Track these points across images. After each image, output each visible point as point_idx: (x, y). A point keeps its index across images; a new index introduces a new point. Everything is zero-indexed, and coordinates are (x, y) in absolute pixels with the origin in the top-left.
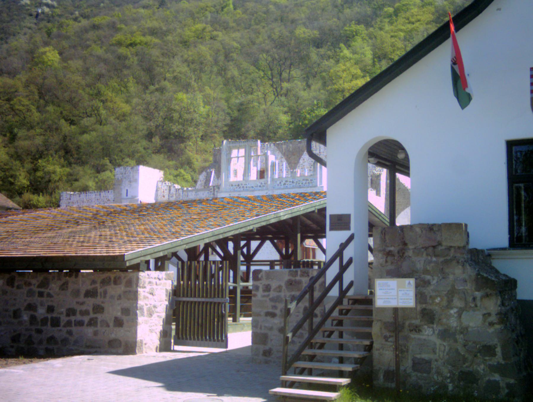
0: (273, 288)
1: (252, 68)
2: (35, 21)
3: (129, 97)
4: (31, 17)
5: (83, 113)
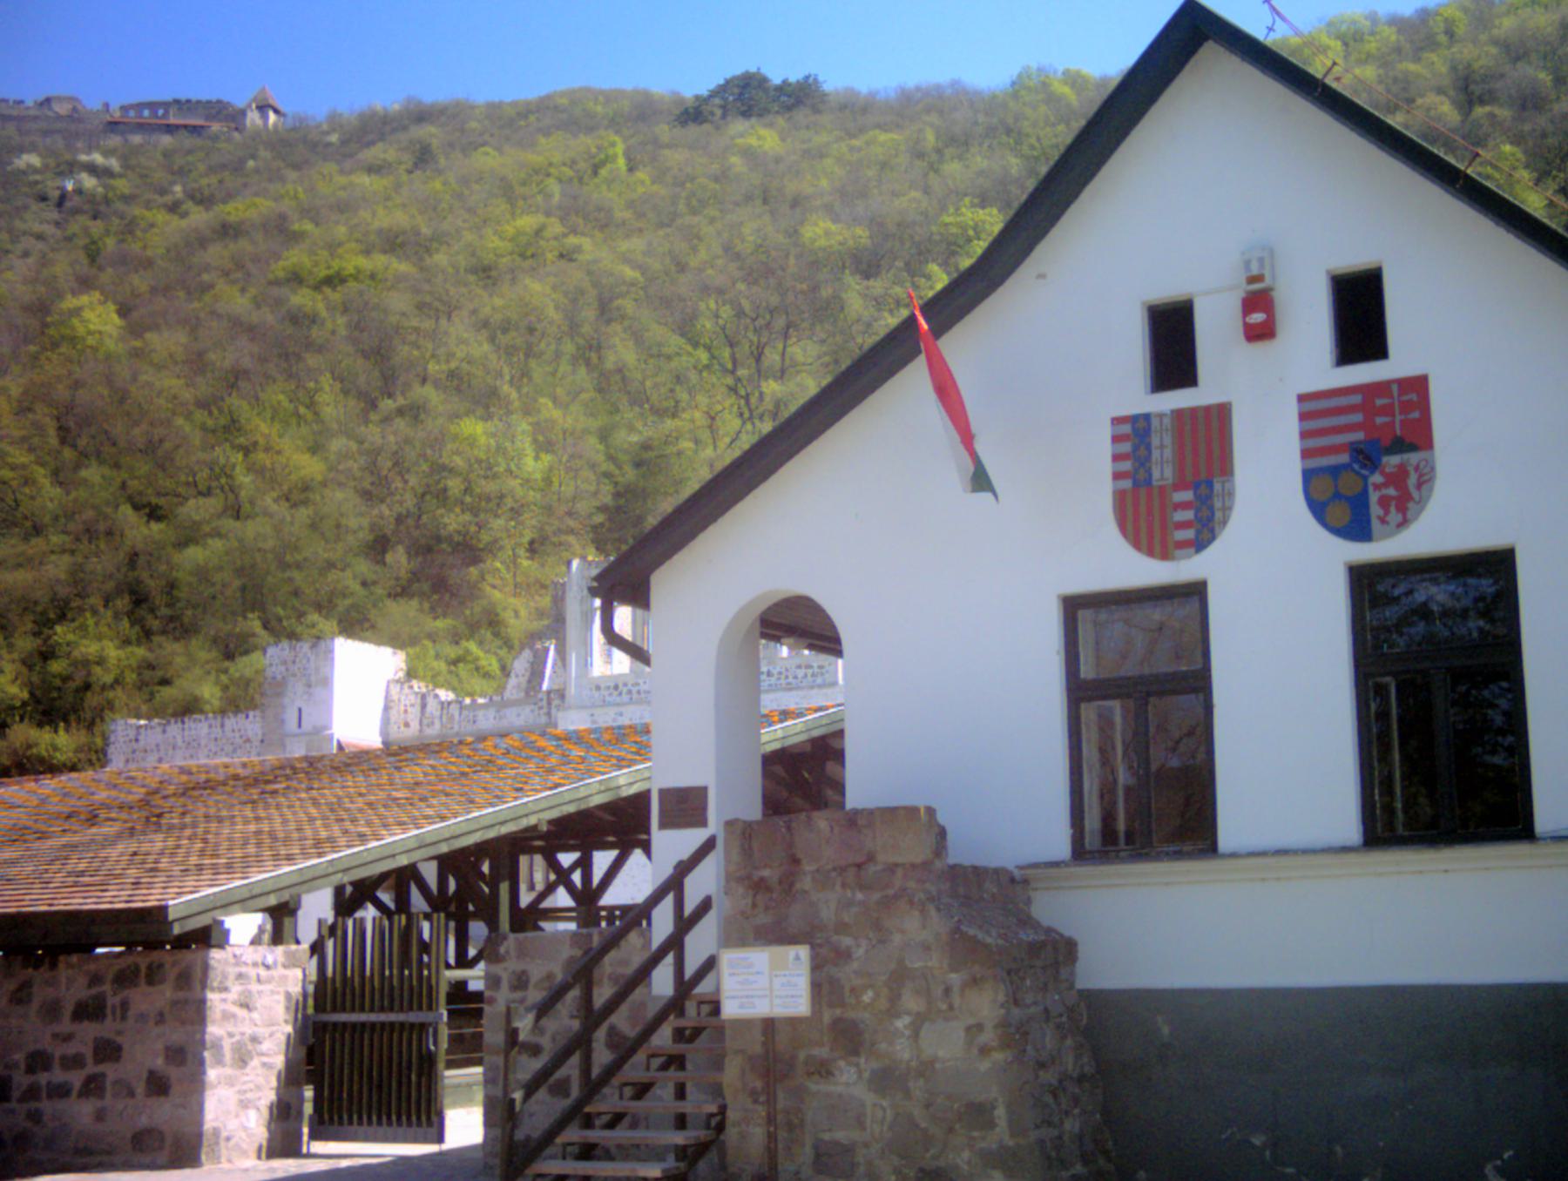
0: (533, 980)
1: (675, 341)
2: (55, 215)
3: (320, 433)
4: (42, 205)
5: (188, 484)
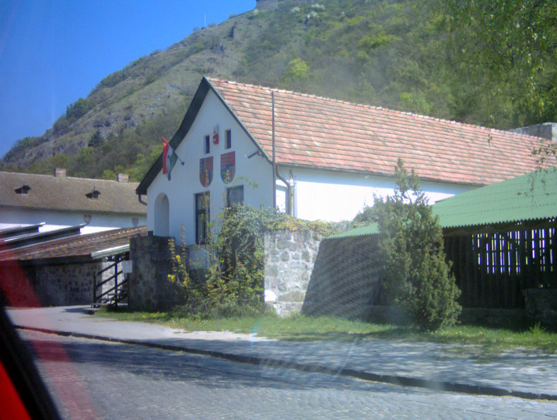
2: (304, 27)
4: (300, 24)
